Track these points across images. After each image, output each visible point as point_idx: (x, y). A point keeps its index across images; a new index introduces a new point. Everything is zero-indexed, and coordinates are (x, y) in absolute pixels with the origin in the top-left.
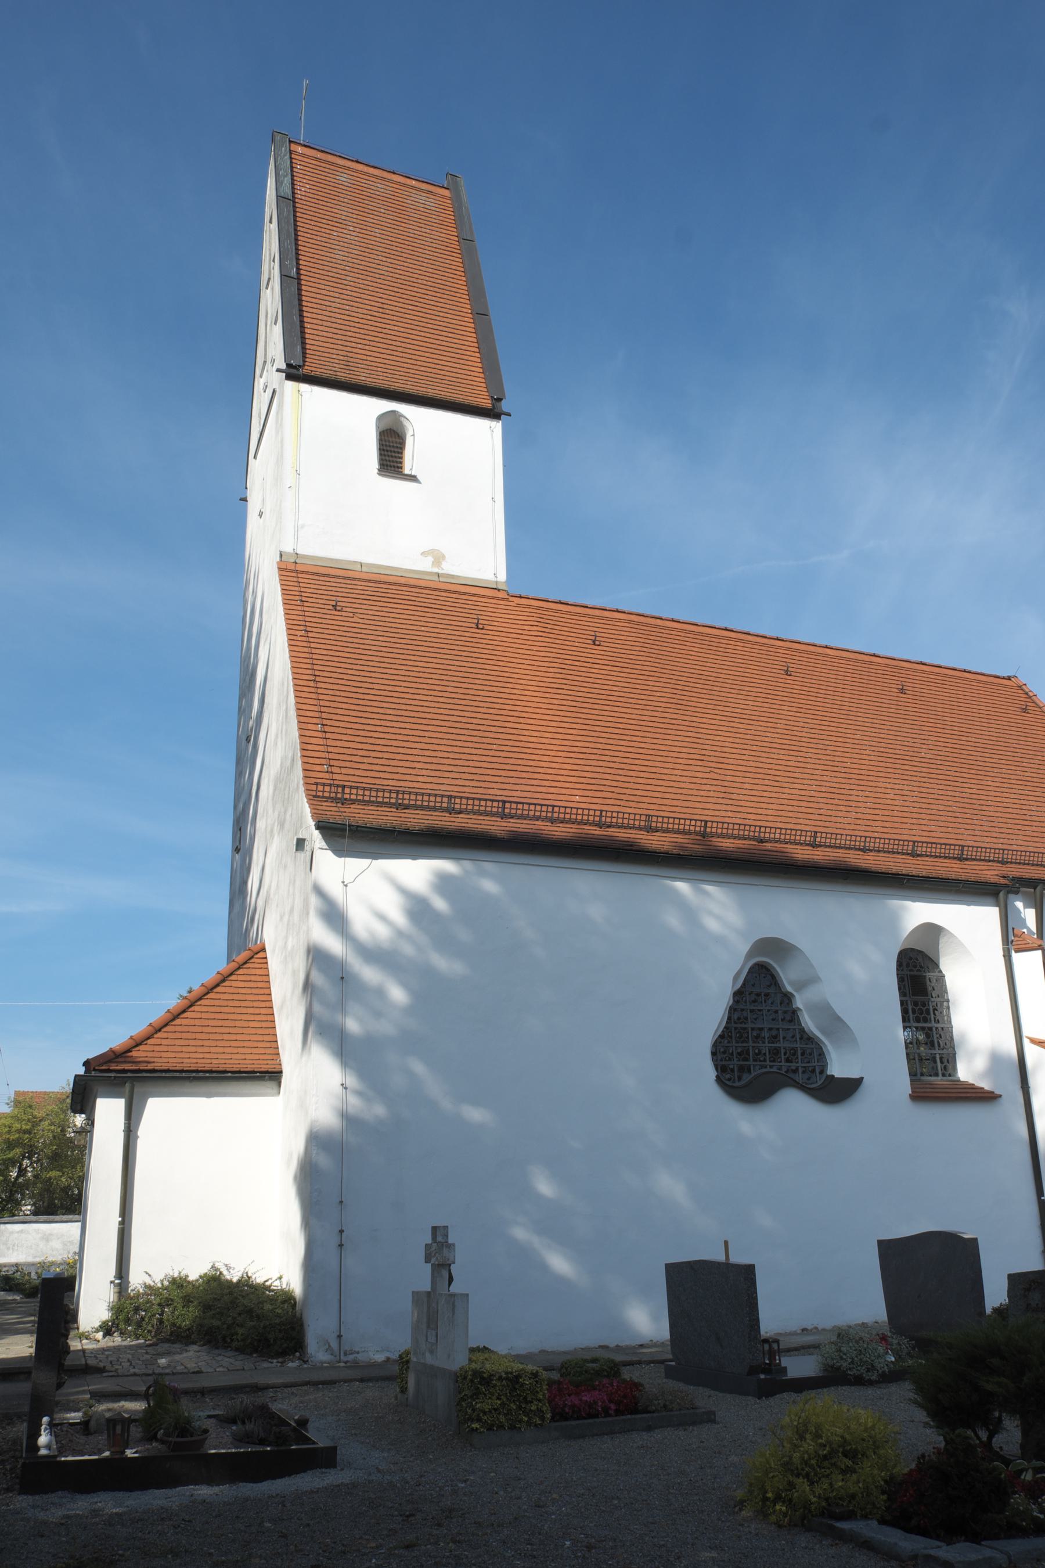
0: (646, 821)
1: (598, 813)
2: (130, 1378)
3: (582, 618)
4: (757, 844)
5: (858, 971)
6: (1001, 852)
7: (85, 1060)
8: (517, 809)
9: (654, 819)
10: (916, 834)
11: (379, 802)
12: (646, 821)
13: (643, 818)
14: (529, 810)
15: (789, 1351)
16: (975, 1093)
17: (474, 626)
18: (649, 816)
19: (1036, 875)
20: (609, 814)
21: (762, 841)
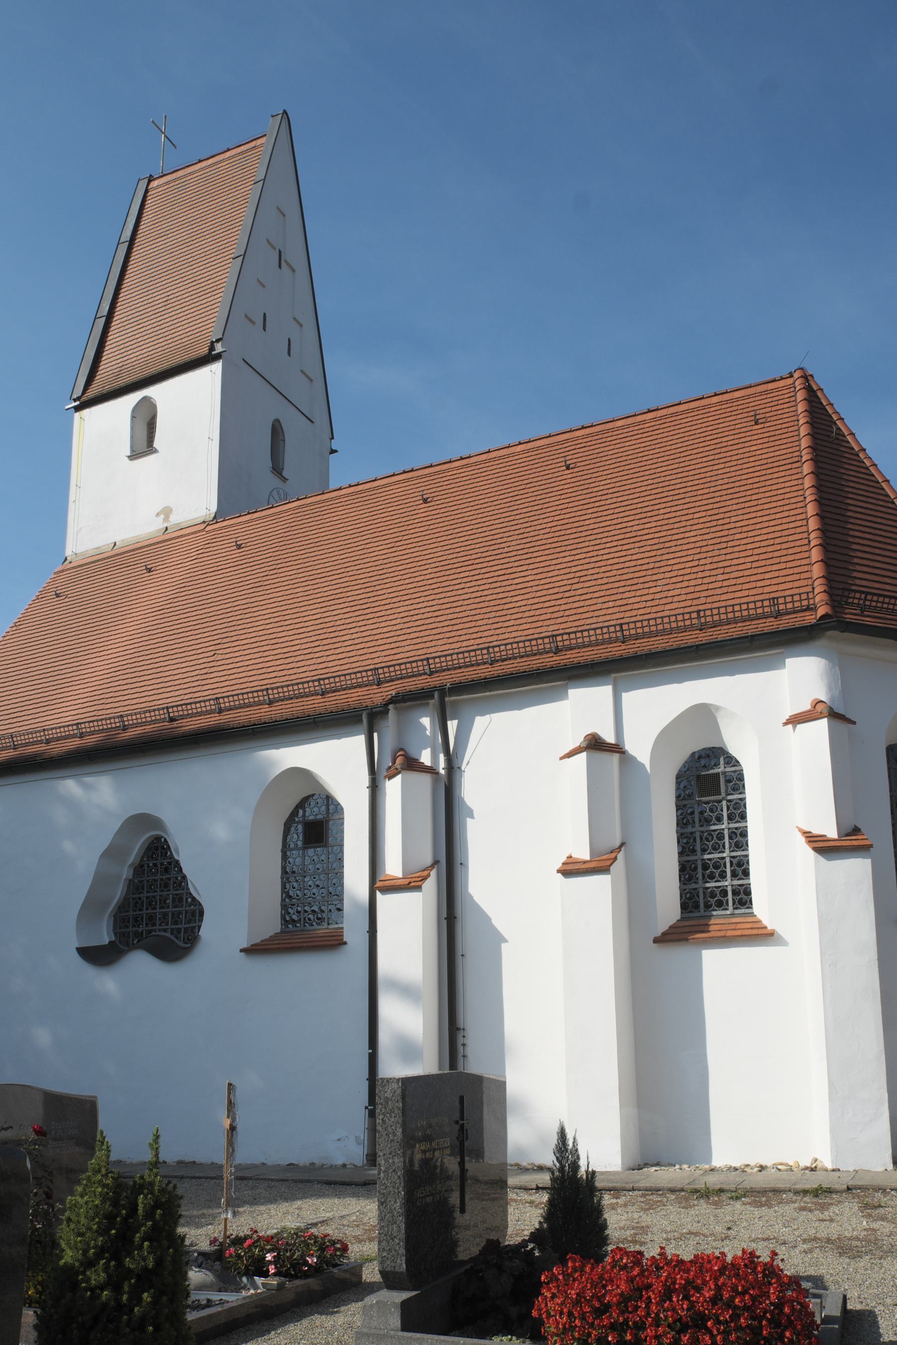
0: (770, 606)
1: (694, 615)
2: (201, 1174)
3: (323, 505)
4: (168, 724)
5: (220, 831)
6: (265, 693)
7: (206, 931)
8: (309, 687)
9: (781, 601)
10: (379, 659)
11: (114, 728)
12: (770, 606)
13: (766, 603)
14: (589, 636)
15: (588, 1168)
16: (289, 943)
17: (235, 548)
18: (773, 599)
19: (508, 670)
20: (708, 613)
21: (172, 720)
